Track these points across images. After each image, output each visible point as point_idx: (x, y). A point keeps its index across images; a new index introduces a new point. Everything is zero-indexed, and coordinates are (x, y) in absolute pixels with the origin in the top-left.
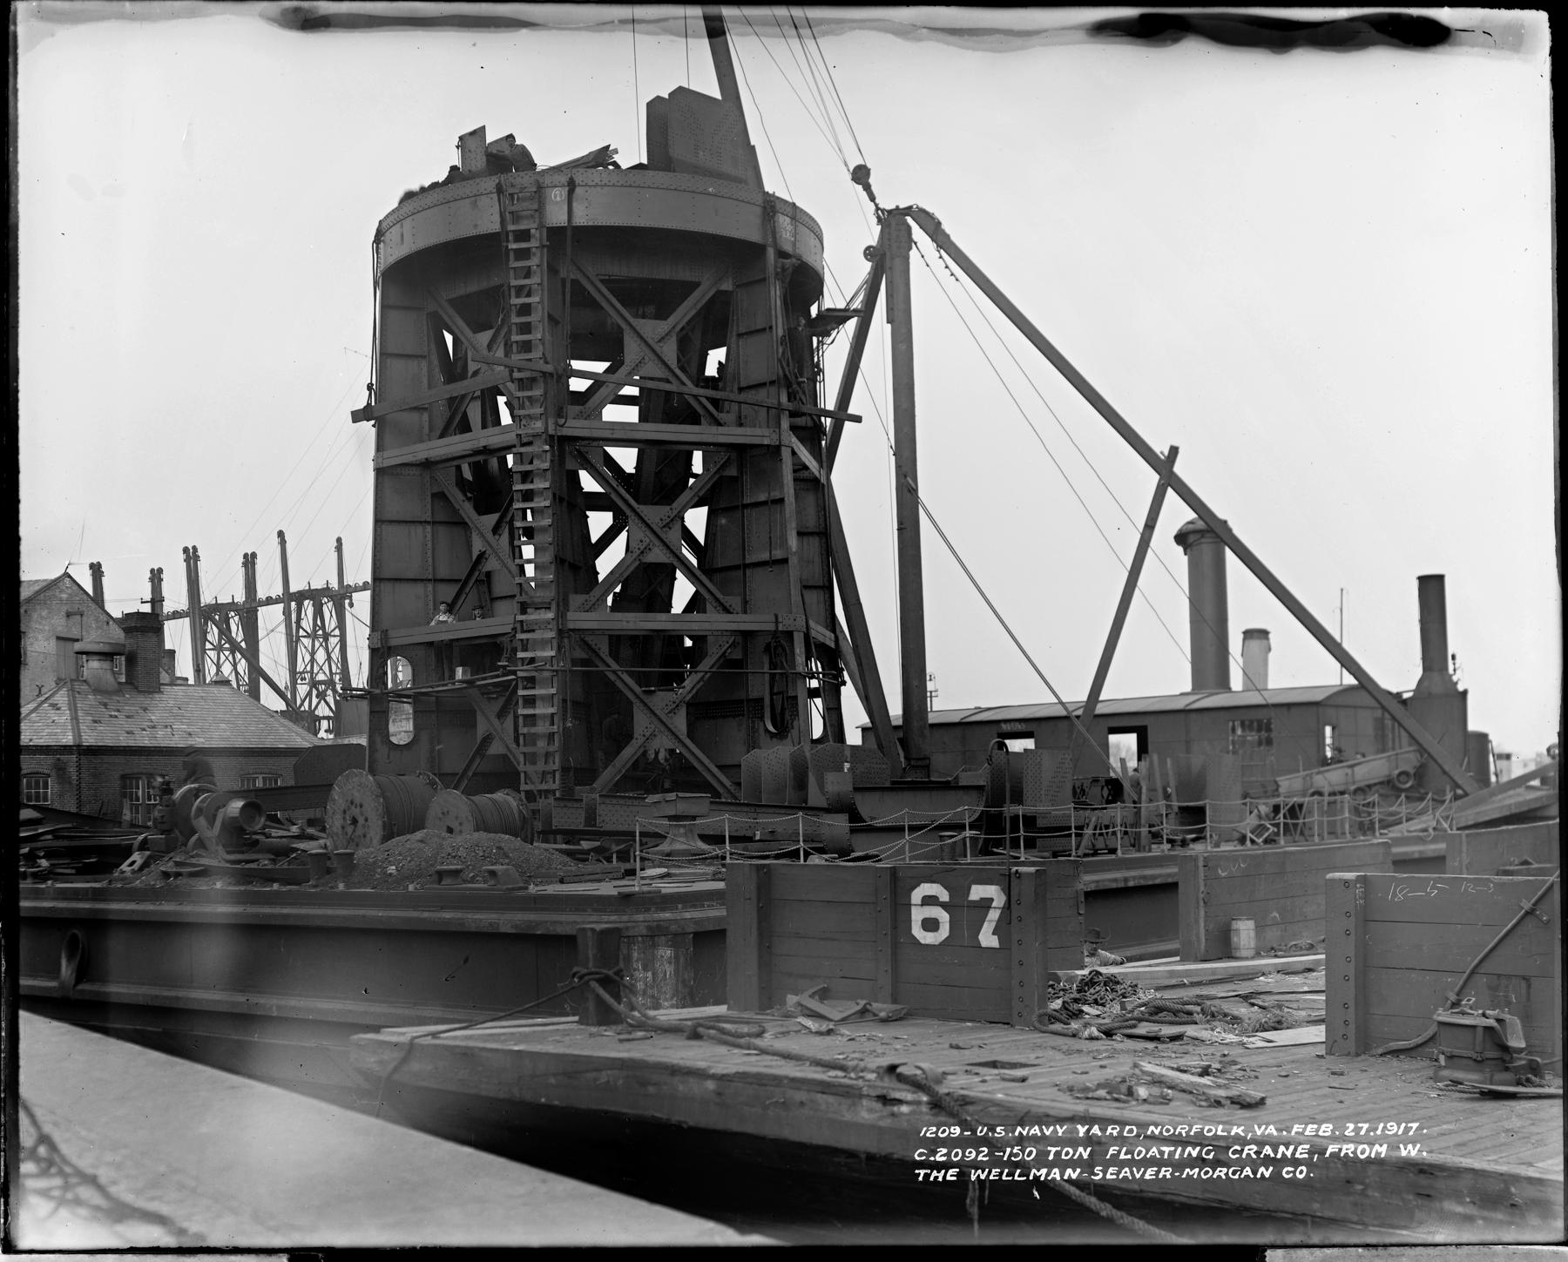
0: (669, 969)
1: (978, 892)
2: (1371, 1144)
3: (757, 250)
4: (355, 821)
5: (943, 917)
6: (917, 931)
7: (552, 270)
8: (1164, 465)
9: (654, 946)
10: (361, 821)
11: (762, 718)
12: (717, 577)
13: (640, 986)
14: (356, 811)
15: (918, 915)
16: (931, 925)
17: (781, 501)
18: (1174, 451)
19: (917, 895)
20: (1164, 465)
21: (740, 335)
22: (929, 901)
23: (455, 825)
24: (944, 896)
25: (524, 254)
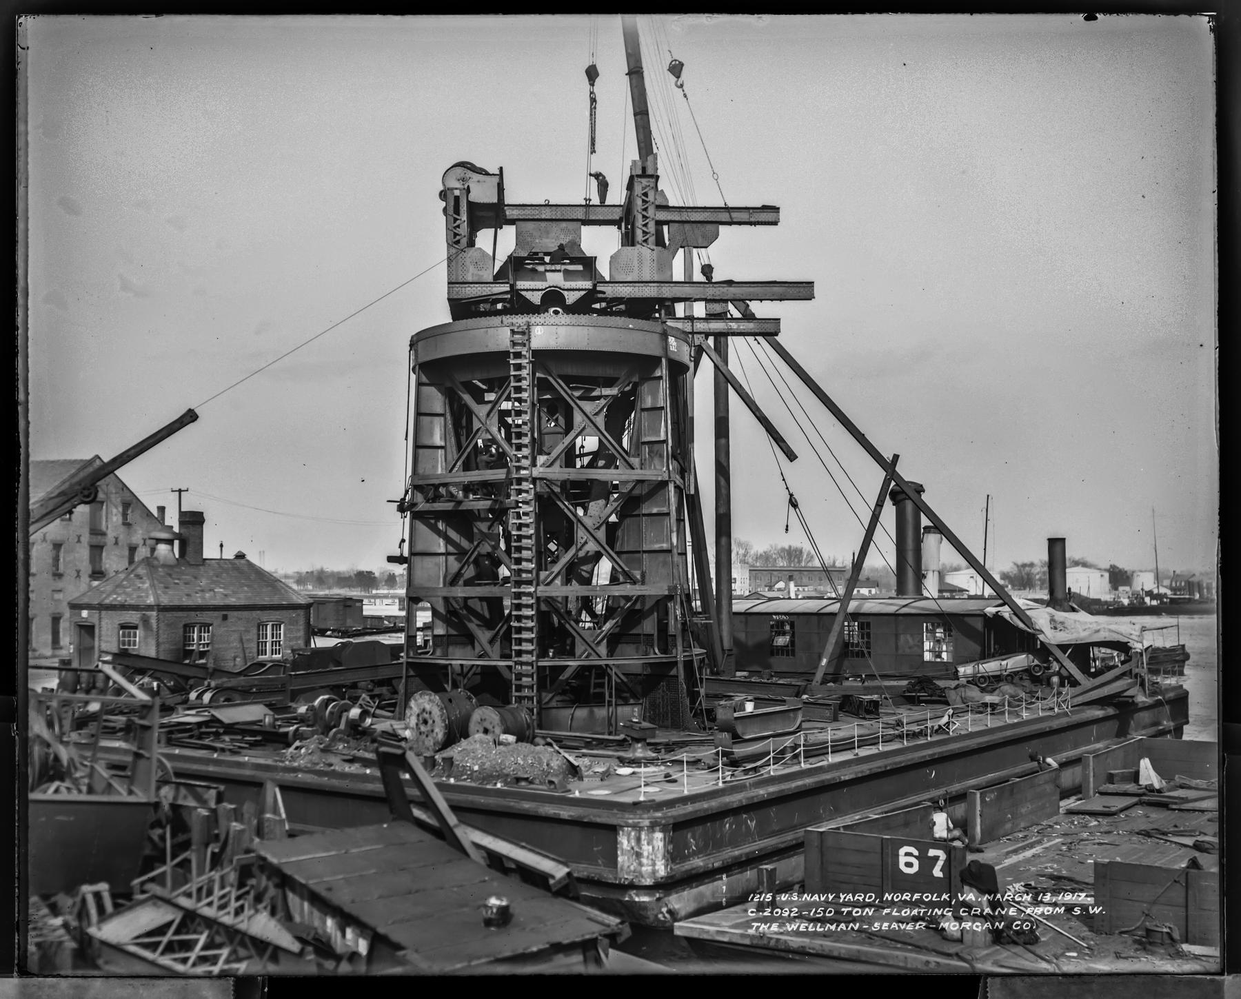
0: (661, 844)
1: (932, 853)
2: (826, 901)
3: (654, 361)
4: (425, 722)
5: (916, 862)
6: (902, 867)
7: (534, 374)
8: (890, 466)
9: (654, 831)
10: (430, 722)
11: (652, 646)
12: (624, 556)
13: (645, 854)
14: (426, 716)
15: (903, 860)
16: (909, 865)
17: (668, 514)
18: (896, 457)
19: (902, 851)
20: (890, 466)
21: (643, 410)
22: (907, 854)
23: (490, 727)
24: (916, 853)
25: (519, 367)
